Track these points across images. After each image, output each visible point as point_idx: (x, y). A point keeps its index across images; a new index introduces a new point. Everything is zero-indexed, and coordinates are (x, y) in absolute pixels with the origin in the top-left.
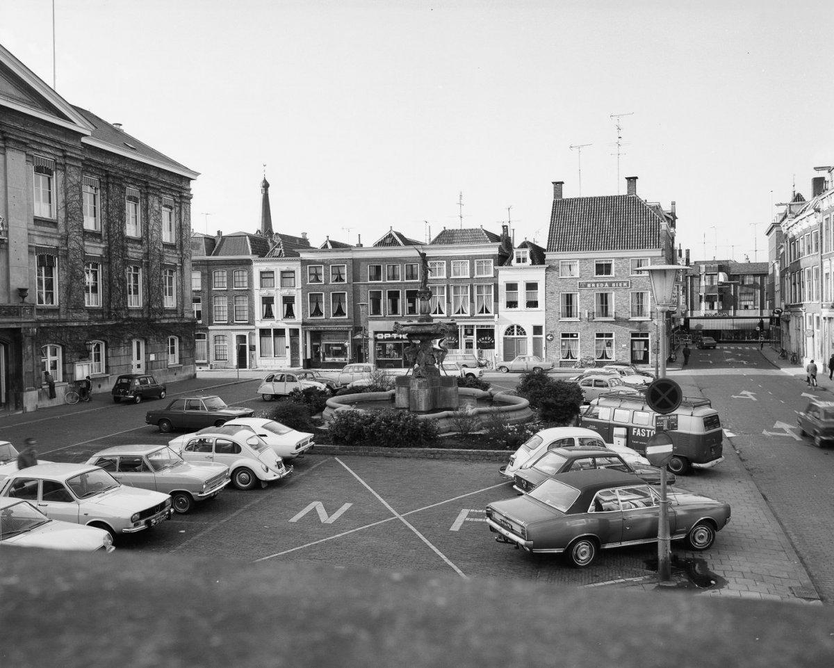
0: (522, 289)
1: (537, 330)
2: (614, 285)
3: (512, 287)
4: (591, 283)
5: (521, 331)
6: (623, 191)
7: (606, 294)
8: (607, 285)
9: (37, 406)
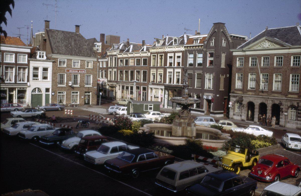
0: (218, 57)
1: (47, 90)
2: (79, 71)
3: (36, 69)
4: (71, 70)
5: (39, 90)
6: (73, 30)
7: (76, 75)
8: (77, 71)
9: (227, 154)
